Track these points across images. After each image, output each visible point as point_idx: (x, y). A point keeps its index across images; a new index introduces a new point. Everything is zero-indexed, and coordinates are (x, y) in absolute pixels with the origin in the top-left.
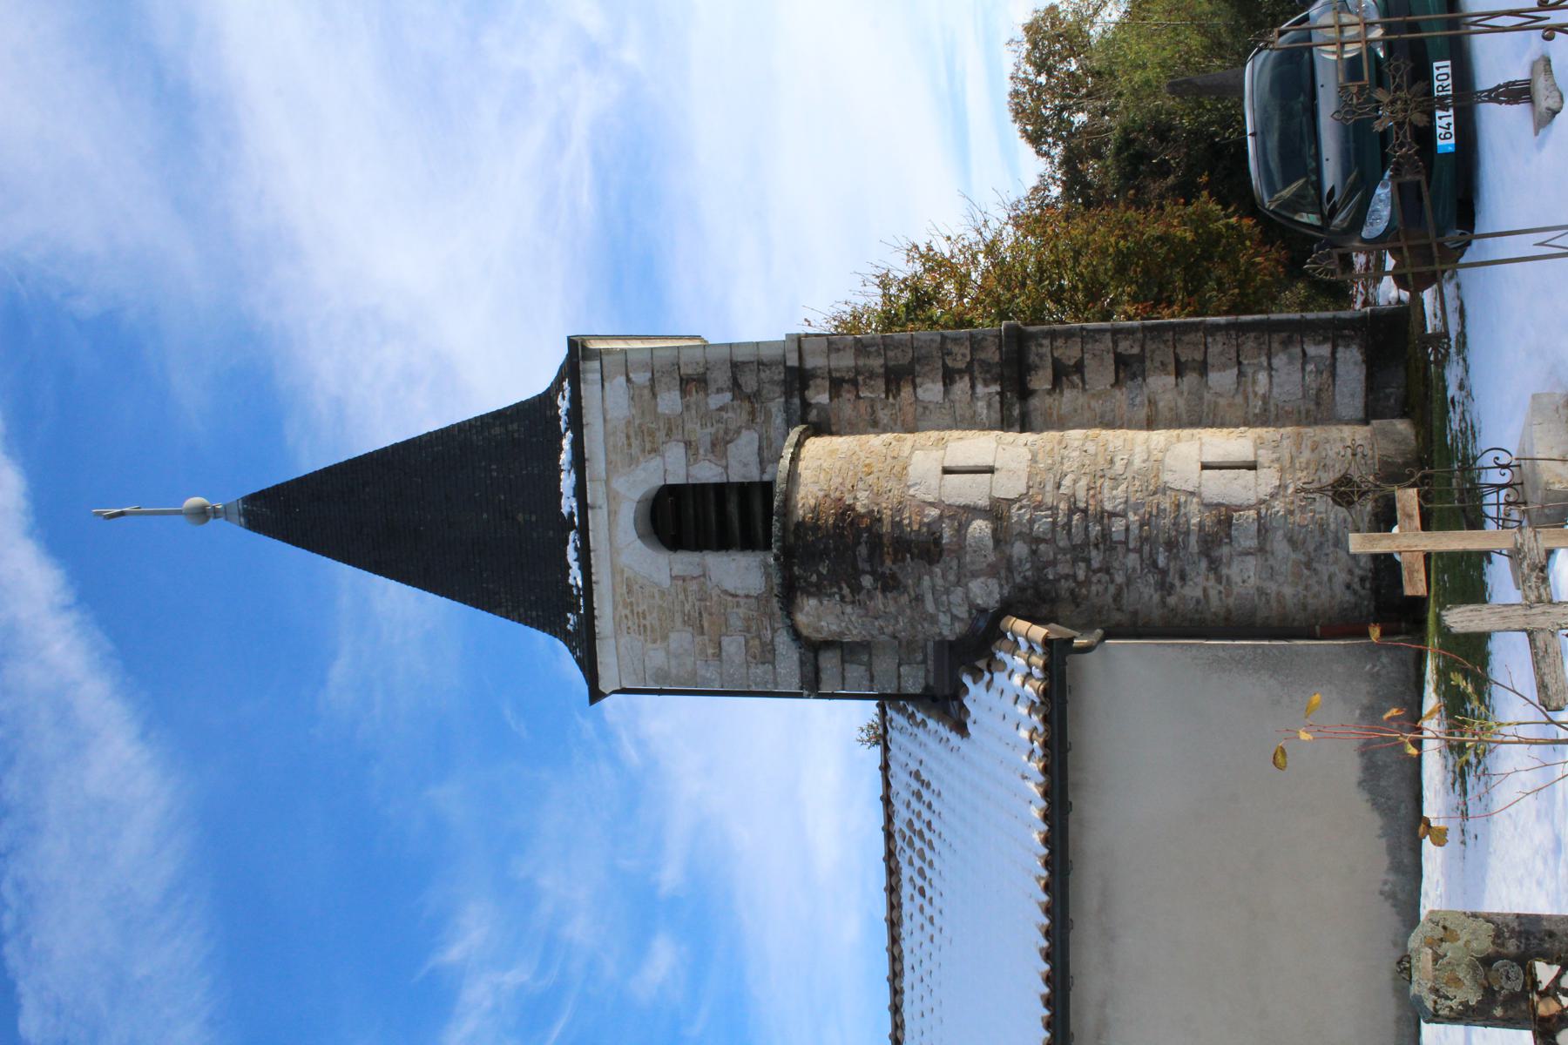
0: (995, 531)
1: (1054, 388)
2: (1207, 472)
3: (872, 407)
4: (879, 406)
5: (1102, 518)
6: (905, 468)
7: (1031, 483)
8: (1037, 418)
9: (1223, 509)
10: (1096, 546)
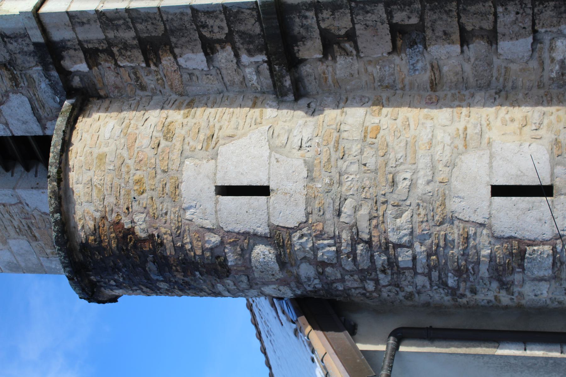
0: (278, 257)
1: (325, 56)
2: (499, 200)
3: (135, 74)
4: (142, 73)
5: (387, 248)
6: (177, 187)
7: (309, 209)
8: (311, 85)
9: (515, 243)
10: (384, 271)
